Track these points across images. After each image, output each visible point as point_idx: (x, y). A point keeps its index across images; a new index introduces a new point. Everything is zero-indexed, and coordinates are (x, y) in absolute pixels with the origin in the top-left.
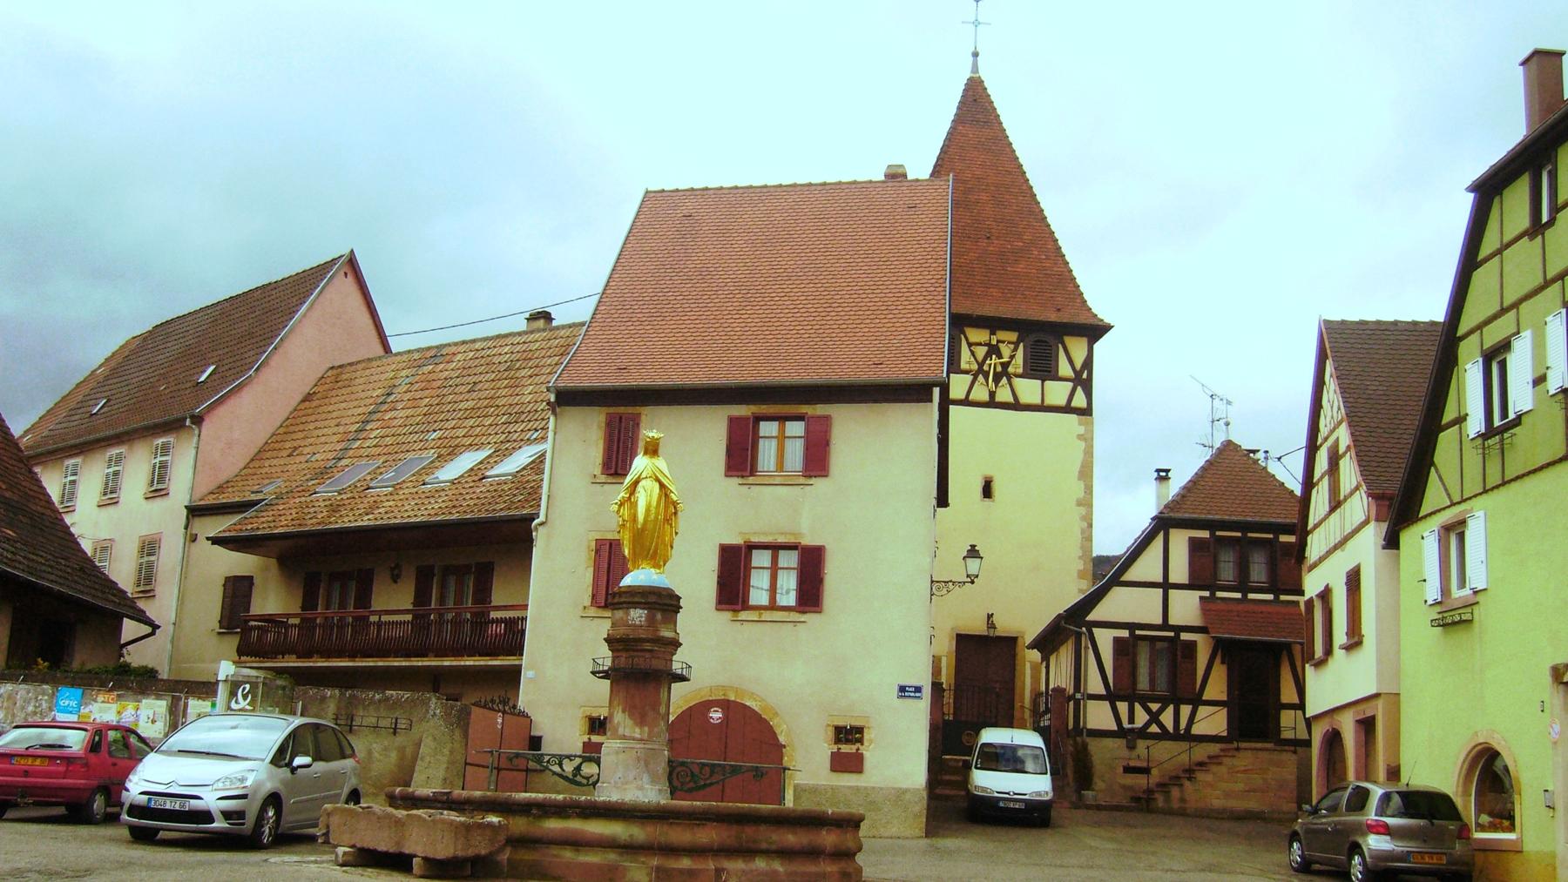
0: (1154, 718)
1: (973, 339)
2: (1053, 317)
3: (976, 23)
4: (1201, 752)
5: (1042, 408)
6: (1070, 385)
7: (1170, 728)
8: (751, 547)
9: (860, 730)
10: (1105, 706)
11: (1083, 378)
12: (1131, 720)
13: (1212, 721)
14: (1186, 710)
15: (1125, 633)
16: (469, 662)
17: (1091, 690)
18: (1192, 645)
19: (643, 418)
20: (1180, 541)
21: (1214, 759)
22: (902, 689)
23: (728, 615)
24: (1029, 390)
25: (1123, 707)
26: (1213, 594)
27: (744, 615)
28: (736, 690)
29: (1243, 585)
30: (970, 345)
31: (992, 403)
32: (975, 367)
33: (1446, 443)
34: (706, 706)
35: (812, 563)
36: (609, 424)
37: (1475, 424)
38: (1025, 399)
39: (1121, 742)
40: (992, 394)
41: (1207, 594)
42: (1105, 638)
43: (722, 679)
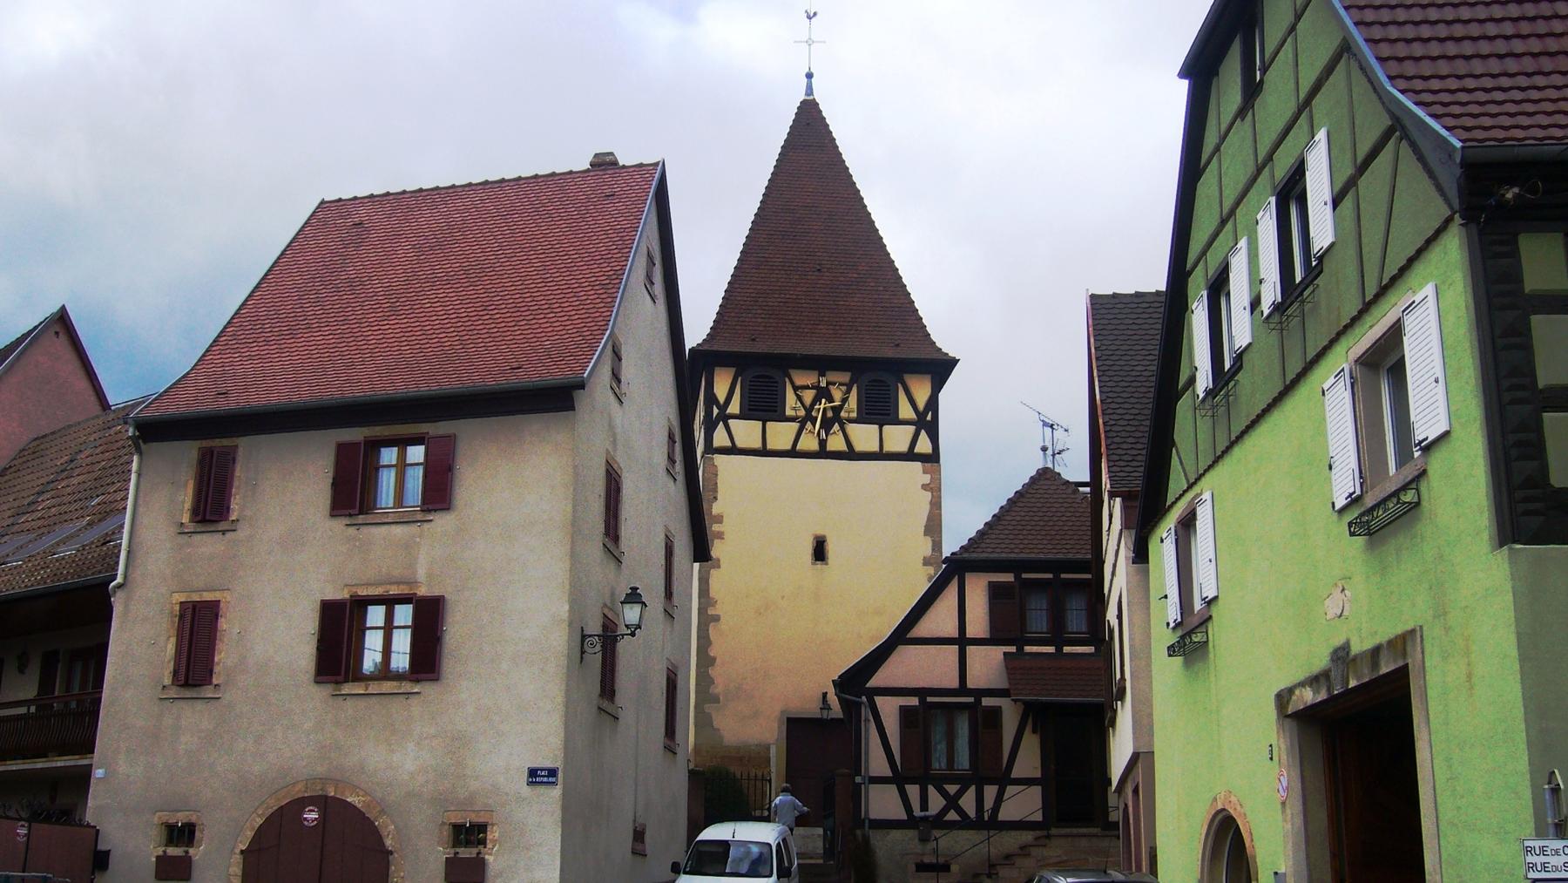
0: (952, 802)
1: (799, 382)
2: (889, 353)
3: (810, 42)
4: (1010, 841)
5: (881, 455)
6: (912, 429)
7: (972, 813)
8: (360, 604)
9: (482, 828)
10: (892, 790)
11: (927, 422)
12: (924, 807)
13: (1023, 804)
14: (990, 792)
15: (914, 701)
16: (40, 764)
17: (873, 773)
18: (996, 712)
19: (241, 453)
20: (977, 591)
21: (1024, 850)
22: (533, 773)
23: (327, 690)
24: (864, 436)
25: (913, 791)
26: (1020, 649)
27: (347, 688)
28: (337, 783)
29: (1058, 637)
30: (796, 388)
31: (823, 453)
32: (802, 413)
33: (1183, 407)
34: (301, 804)
35: (430, 617)
36: (201, 462)
37: (1204, 381)
38: (859, 447)
39: (911, 834)
40: (823, 443)
41: (1013, 649)
42: (889, 708)
43: (320, 770)
